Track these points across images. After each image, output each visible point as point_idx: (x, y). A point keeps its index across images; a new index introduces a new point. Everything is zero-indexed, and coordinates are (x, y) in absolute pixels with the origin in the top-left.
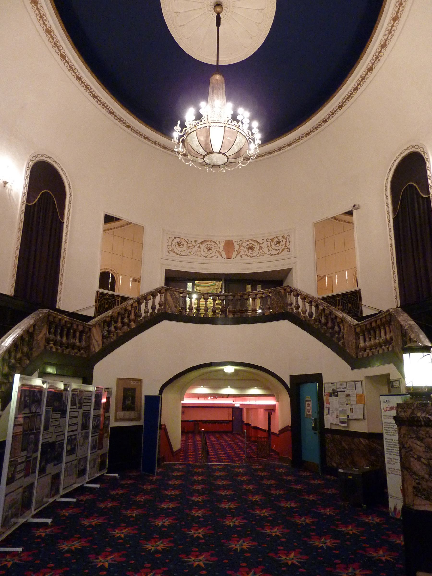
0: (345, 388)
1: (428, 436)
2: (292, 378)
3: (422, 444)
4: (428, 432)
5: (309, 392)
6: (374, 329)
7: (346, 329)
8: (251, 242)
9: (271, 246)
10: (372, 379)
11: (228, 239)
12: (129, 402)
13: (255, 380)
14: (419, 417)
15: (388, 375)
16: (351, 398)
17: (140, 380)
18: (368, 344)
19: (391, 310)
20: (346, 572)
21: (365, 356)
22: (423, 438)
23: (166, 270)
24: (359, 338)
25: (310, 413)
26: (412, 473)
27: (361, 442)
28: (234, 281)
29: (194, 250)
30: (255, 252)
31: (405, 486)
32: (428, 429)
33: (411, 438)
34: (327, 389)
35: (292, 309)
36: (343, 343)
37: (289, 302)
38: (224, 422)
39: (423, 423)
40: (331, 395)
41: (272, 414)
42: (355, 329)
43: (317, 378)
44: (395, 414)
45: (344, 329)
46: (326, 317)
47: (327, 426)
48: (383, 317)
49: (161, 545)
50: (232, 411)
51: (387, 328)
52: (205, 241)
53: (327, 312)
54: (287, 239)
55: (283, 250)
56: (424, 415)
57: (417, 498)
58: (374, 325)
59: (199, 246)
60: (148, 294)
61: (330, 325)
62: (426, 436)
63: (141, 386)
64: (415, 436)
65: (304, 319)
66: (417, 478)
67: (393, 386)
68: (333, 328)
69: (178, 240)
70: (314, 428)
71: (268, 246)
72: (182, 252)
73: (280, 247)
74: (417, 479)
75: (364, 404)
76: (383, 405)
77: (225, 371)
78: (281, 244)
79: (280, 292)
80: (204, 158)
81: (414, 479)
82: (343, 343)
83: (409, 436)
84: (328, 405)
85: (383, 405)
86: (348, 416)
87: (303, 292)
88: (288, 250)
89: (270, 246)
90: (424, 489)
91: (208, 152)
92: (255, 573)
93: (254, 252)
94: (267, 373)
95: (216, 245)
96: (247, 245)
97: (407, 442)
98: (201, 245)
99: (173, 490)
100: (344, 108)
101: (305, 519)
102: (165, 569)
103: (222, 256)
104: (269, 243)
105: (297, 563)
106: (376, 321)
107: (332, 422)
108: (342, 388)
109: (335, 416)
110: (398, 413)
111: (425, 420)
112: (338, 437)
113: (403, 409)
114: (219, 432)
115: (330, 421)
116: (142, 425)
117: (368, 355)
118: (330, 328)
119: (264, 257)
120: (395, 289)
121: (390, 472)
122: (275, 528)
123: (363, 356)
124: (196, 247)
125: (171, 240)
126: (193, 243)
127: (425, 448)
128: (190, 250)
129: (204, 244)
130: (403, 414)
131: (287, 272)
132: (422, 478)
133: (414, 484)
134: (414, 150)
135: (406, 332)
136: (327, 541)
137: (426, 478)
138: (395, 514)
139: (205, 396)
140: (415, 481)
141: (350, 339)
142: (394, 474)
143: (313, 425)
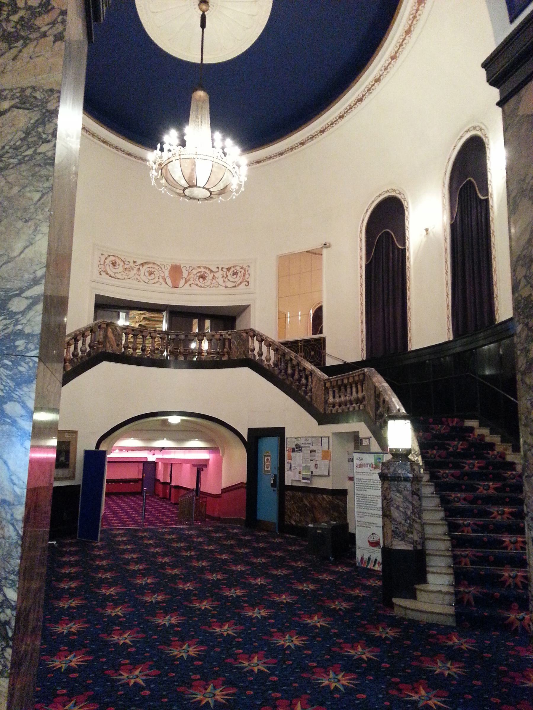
0: (310, 444)
2: (250, 430)
5: (268, 446)
6: (345, 386)
7: (314, 383)
8: (203, 269)
9: (227, 276)
11: (177, 263)
12: (62, 459)
13: (197, 431)
14: (400, 474)
16: (316, 454)
17: (76, 432)
18: (337, 400)
20: (283, 639)
21: (333, 412)
23: (97, 296)
24: (328, 393)
25: (269, 469)
27: (323, 499)
28: (181, 315)
29: (132, 273)
30: (208, 282)
31: (385, 530)
32: (406, 483)
34: (290, 444)
35: (254, 356)
36: (311, 397)
37: (252, 347)
38: (121, 481)
40: (293, 450)
41: (203, 470)
42: (325, 384)
43: (279, 432)
44: (380, 471)
45: (312, 383)
46: (293, 367)
47: (288, 482)
49: (75, 660)
50: (143, 466)
51: (359, 387)
52: (146, 263)
53: (295, 362)
54: (246, 270)
55: (241, 283)
56: (403, 472)
57: (395, 539)
58: (345, 381)
59: (139, 269)
60: (86, 329)
61: (296, 376)
63: (76, 439)
65: (267, 368)
68: (299, 380)
69: (112, 258)
70: (273, 485)
71: (223, 277)
72: (116, 275)
73: (238, 279)
77: (169, 421)
78: (238, 276)
79: (241, 335)
80: (184, 191)
81: (393, 524)
82: (311, 397)
84: (290, 461)
86: (312, 472)
87: (263, 335)
88: (247, 284)
89: (225, 276)
90: (400, 532)
91: (191, 185)
92: (75, 705)
93: (205, 281)
94: (220, 424)
95: (160, 269)
96: (198, 272)
98: (141, 268)
99: (70, 581)
100: (325, 133)
101: (235, 590)
102: (90, 693)
103: (166, 283)
104: (225, 273)
105: (233, 634)
106: (348, 379)
107: (293, 479)
108: (307, 444)
109: (298, 472)
110: (382, 470)
112: (299, 494)
114: (125, 494)
115: (291, 478)
116: (80, 485)
118: (297, 380)
119: (217, 289)
120: (362, 341)
122: (204, 602)
124: (135, 269)
125: (103, 258)
126: (132, 264)
128: (127, 272)
129: (146, 266)
130: (386, 471)
131: (243, 309)
132: (400, 523)
133: (393, 528)
134: (393, 194)
135: (380, 394)
136: (261, 612)
138: (362, 563)
139: (133, 449)
141: (318, 392)
142: (363, 527)
143: (272, 482)
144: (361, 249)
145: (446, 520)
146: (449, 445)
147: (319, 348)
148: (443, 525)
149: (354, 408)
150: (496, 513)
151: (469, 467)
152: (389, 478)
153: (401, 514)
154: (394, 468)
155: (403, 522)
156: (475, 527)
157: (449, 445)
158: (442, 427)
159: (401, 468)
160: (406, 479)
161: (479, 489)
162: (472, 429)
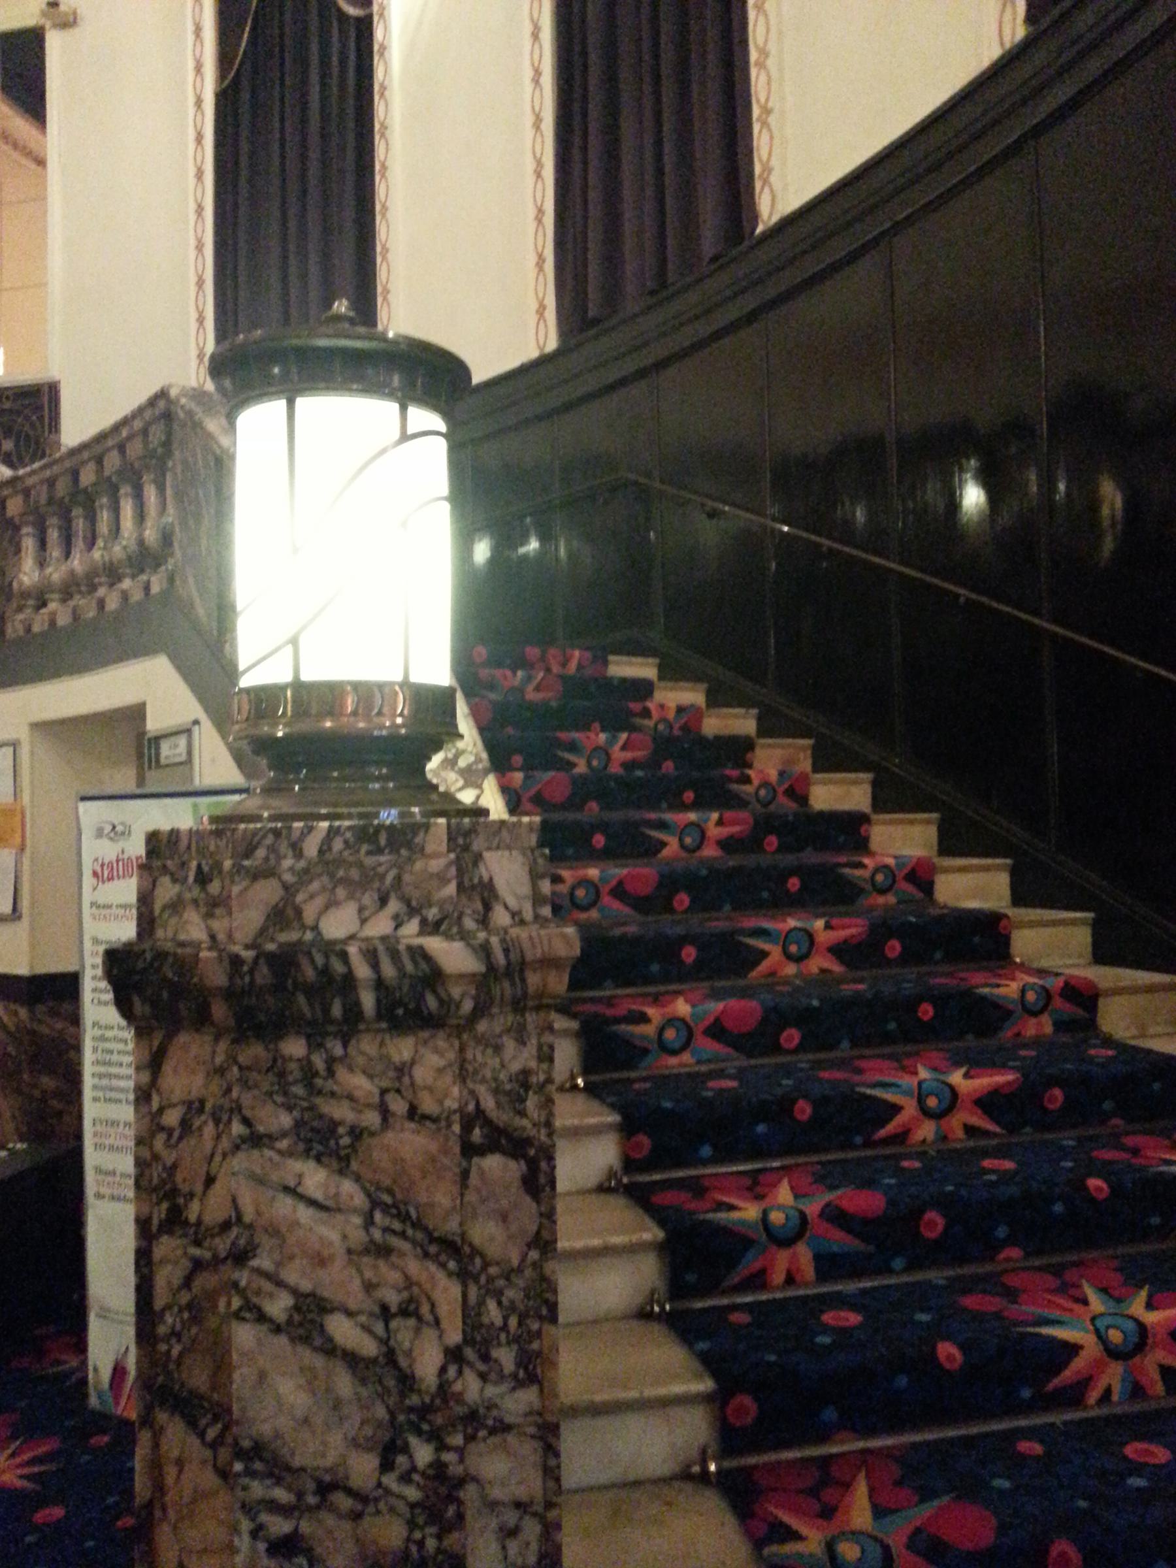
1: (398, 1106)
3: (348, 1187)
4: (403, 1070)
10: (62, 732)
14: (337, 950)
15: (136, 714)
18: (56, 573)
19: (173, 393)
21: (36, 629)
22: (357, 1133)
26: (239, 1453)
32: (402, 1048)
33: (256, 1140)
39: (368, 1000)
48: (130, 438)
56: (380, 926)
62: (385, 1113)
64: (286, 1120)
66: (281, 1495)
67: (158, 755)
74: (273, 1506)
75: (22, 849)
76: (95, 850)
83: (237, 1128)
85: (95, 850)
97: (210, 1181)
110: (147, 922)
111: (388, 970)
113: (203, 879)
117: (53, 623)
121: (103, 1190)
123: (28, 630)
127: (369, 1222)
130: (194, 928)
132: (325, 1489)
137: (356, 1482)
138: (117, 1404)
140: (256, 1532)
144: (198, 30)
145: (640, 1196)
146: (573, 747)
147: (33, 425)
148: (632, 1249)
149: (125, 596)
150: (910, 1109)
151: (682, 846)
152: (219, 1011)
153: (344, 1384)
154: (267, 892)
155: (363, 1468)
156: (839, 1241)
157: (573, 747)
158: (529, 678)
159: (355, 887)
160: (414, 1001)
161: (764, 954)
162: (642, 689)
